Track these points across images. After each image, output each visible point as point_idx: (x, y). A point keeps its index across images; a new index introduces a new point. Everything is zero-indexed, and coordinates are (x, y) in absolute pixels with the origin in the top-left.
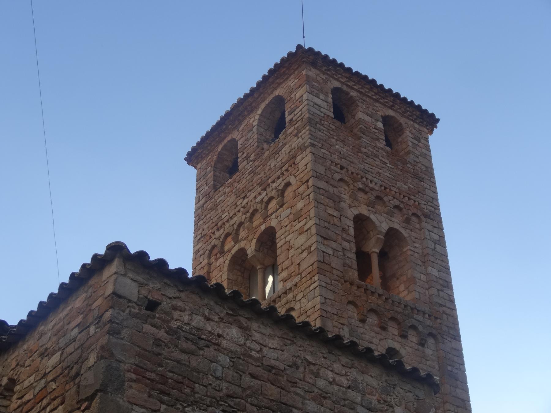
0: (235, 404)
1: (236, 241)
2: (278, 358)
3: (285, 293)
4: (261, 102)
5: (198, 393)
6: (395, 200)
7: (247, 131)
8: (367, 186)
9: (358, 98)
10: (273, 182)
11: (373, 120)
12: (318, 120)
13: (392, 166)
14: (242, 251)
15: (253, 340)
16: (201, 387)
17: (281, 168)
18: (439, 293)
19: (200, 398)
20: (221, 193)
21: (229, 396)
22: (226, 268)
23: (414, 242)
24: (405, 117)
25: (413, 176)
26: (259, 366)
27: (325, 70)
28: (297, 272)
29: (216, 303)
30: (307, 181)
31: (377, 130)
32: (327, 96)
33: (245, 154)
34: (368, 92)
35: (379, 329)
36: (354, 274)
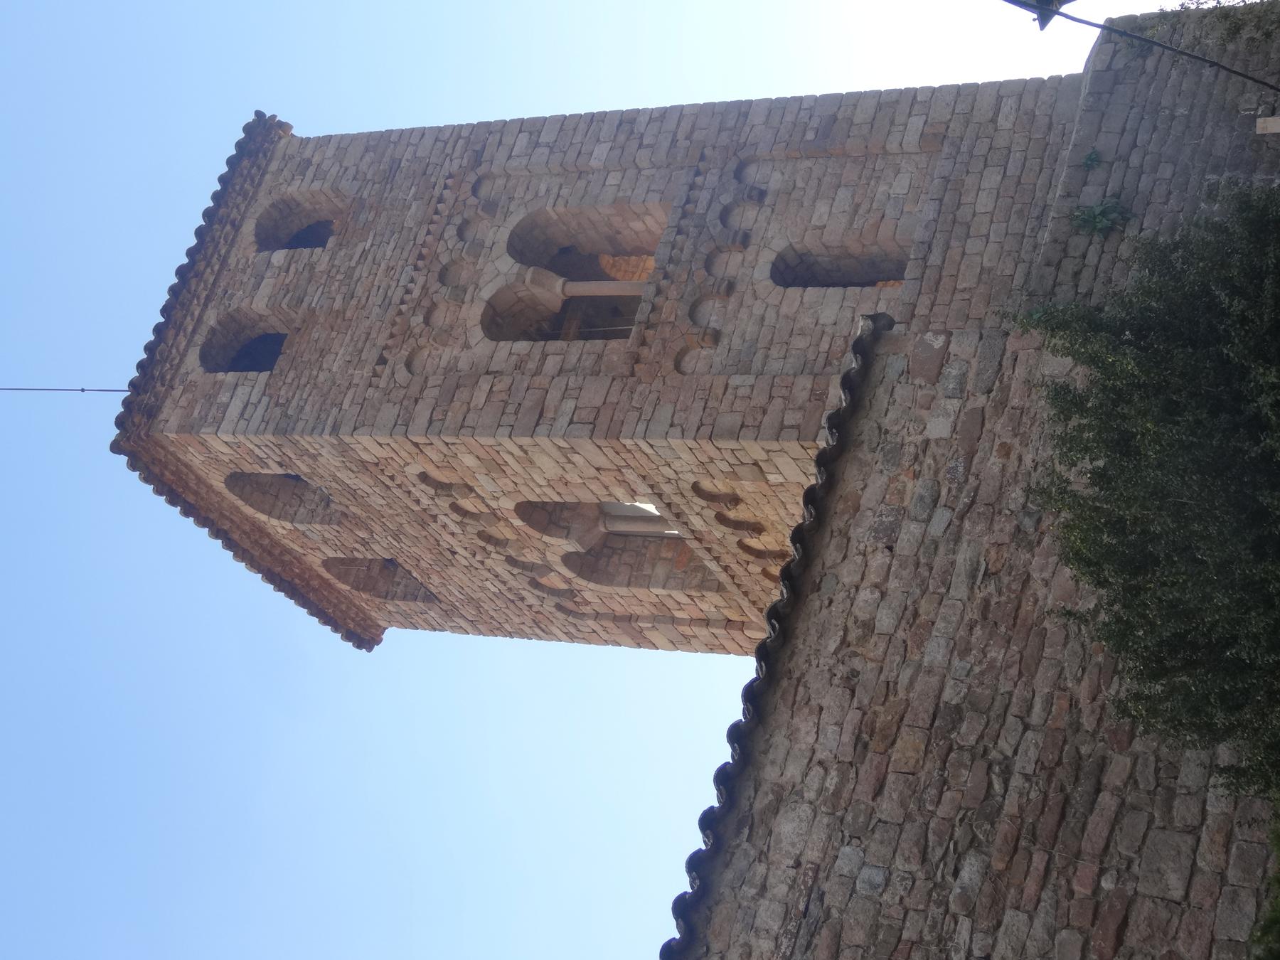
0: (941, 845)
1: (548, 568)
2: (836, 724)
3: (660, 496)
4: (241, 513)
5: (921, 932)
6: (446, 236)
7: (305, 540)
8: (419, 303)
9: (222, 308)
10: (418, 502)
11: (269, 274)
12: (278, 411)
13: (371, 237)
14: (568, 559)
15: (803, 782)
16: (908, 924)
17: (388, 487)
18: (648, 146)
19: (933, 928)
20: (443, 590)
21: (924, 860)
22: (607, 589)
23: (536, 195)
24: (255, 193)
25: (389, 186)
26: (857, 774)
27: (163, 385)
28: (617, 473)
29: (727, 865)
30: (416, 445)
31: (290, 264)
32: (222, 383)
33: (357, 546)
34: (206, 282)
35: (732, 299)
36: (616, 350)
